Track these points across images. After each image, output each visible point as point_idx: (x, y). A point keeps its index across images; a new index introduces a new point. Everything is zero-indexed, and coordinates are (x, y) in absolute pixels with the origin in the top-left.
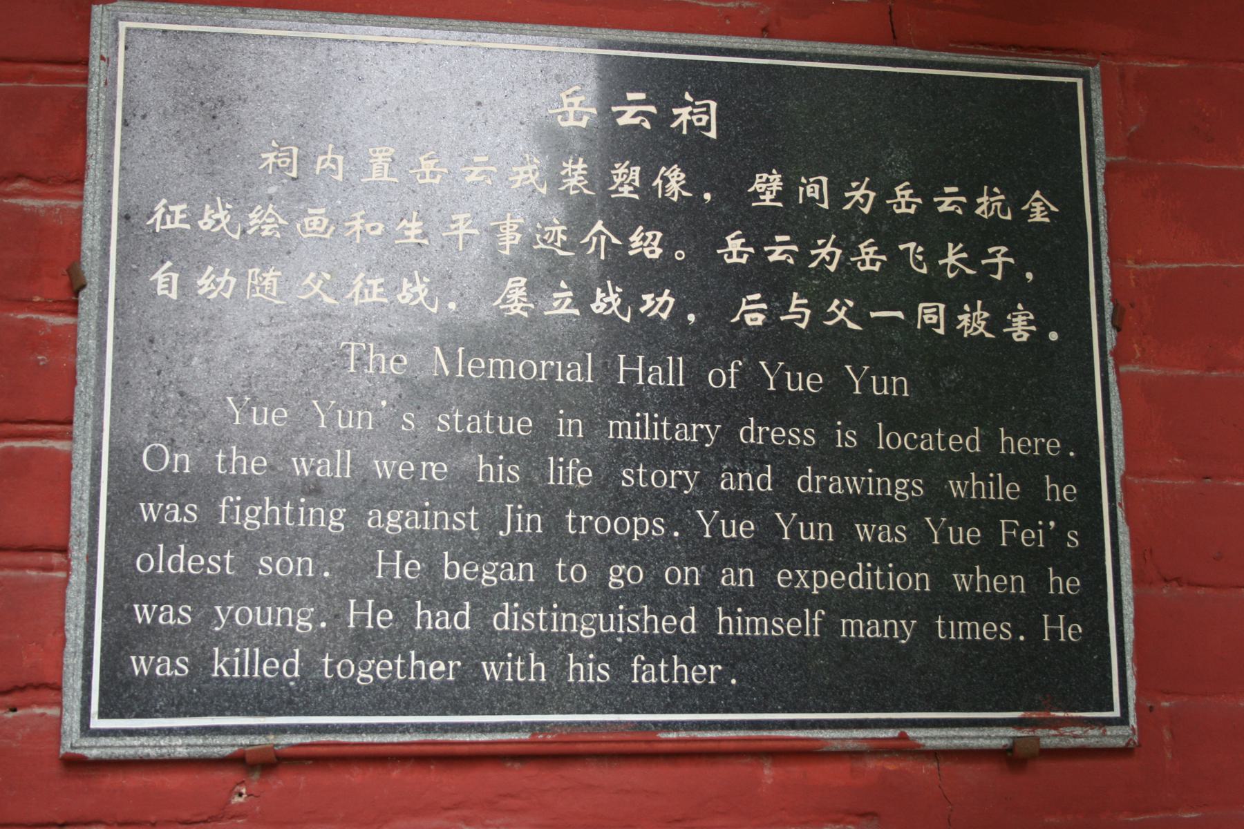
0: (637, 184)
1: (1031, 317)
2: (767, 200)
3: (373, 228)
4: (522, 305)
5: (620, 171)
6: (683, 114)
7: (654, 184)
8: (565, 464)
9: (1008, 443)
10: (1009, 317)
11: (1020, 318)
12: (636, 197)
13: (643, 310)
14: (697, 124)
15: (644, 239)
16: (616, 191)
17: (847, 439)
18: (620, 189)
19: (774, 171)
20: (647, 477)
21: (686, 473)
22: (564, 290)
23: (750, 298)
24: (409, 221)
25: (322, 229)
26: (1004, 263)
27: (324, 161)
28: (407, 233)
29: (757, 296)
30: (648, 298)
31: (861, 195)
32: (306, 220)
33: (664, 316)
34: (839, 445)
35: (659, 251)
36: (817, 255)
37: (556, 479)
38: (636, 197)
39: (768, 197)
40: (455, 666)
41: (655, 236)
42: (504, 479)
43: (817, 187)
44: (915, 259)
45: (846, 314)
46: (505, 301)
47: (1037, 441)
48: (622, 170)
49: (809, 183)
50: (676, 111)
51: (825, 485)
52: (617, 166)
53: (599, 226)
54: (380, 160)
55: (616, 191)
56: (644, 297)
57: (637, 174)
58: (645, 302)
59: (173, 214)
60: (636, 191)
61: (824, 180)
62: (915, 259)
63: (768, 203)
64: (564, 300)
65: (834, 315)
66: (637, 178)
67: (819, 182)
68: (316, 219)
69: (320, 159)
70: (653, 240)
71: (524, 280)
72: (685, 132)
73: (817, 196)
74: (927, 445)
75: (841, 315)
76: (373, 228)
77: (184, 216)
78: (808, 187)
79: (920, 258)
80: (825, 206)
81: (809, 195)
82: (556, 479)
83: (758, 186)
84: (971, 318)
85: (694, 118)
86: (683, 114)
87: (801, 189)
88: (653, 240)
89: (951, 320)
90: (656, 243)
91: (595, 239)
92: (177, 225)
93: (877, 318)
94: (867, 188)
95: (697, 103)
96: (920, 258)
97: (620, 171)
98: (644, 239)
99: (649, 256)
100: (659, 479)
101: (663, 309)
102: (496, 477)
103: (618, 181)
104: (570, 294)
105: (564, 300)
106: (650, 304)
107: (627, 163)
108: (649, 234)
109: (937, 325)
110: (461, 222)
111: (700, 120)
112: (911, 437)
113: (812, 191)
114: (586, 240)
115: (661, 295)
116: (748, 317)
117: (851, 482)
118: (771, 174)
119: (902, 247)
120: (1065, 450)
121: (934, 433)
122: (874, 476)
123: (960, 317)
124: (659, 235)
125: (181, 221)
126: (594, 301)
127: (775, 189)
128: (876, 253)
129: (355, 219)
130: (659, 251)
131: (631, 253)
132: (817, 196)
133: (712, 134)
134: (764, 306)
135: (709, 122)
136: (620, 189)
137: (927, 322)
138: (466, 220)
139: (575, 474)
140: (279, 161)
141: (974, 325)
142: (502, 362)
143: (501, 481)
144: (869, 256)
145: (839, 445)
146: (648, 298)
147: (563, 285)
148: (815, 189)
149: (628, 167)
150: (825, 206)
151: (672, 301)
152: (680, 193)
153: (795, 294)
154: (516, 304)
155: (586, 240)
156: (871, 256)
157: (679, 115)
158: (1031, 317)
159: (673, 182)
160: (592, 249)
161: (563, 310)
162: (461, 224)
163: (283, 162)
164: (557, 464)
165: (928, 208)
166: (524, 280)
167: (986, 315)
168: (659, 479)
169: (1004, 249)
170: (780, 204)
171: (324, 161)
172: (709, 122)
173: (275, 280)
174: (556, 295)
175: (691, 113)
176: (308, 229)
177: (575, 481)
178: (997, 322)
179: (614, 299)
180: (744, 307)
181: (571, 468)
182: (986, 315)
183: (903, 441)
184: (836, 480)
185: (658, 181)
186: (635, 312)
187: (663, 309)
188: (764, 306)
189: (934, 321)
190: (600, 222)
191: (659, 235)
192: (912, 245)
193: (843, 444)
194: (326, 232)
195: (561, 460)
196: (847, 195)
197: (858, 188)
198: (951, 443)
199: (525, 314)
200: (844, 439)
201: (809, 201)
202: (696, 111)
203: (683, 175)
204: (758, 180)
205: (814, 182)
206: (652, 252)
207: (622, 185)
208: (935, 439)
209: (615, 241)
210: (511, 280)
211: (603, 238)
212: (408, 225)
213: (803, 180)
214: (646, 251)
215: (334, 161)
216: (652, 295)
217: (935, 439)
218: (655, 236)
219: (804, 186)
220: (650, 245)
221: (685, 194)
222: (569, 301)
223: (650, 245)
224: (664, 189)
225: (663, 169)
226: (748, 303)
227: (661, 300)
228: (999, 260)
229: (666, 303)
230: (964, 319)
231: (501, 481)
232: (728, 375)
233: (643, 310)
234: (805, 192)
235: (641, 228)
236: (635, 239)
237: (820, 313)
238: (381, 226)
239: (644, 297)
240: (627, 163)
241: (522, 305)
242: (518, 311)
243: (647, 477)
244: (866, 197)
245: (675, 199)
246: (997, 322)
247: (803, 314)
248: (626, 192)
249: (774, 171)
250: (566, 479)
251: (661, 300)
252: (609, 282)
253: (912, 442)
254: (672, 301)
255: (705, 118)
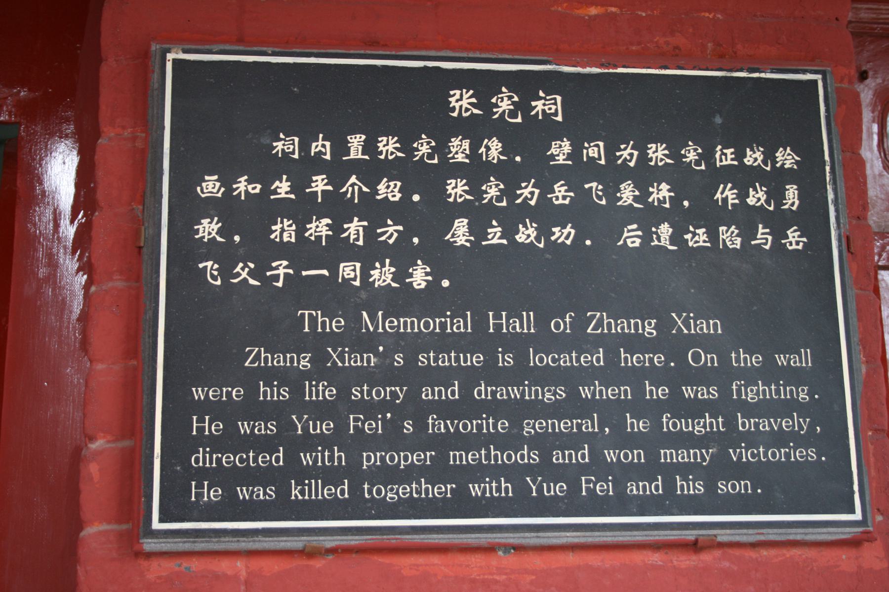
0: (468, 152)
1: (428, 270)
2: (561, 160)
3: (254, 188)
4: (465, 238)
5: (455, 144)
6: (539, 105)
7: (480, 152)
8: (317, 386)
9: (626, 359)
10: (411, 270)
11: (420, 271)
12: (467, 161)
13: (553, 238)
14: (548, 112)
15: (388, 187)
16: (453, 158)
17: (506, 360)
18: (456, 156)
19: (565, 139)
20: (369, 393)
21: (398, 388)
22: (495, 227)
23: (630, 227)
24: (281, 182)
25: (215, 191)
26: (323, 191)
27: (317, 147)
28: (279, 191)
29: (635, 226)
30: (556, 230)
31: (627, 153)
32: (204, 184)
33: (568, 242)
34: (501, 364)
35: (399, 196)
36: (522, 194)
37: (311, 396)
38: (467, 161)
39: (561, 157)
40: (431, 455)
41: (396, 185)
42: (278, 397)
43: (596, 149)
44: (597, 195)
45: (248, 274)
46: (453, 236)
47: (647, 356)
48: (457, 142)
49: (590, 147)
50: (533, 104)
51: (494, 393)
52: (453, 140)
53: (353, 179)
54: (356, 144)
55: (453, 158)
56: (554, 229)
57: (467, 144)
58: (554, 234)
59: (726, 155)
60: (467, 157)
61: (601, 144)
62: (597, 195)
63: (561, 162)
64: (496, 233)
65: (238, 274)
66: (467, 148)
67: (597, 146)
68: (211, 183)
69: (314, 145)
70: (395, 187)
71: (466, 221)
72: (540, 117)
73: (596, 156)
74: (565, 362)
75: (244, 275)
76: (254, 188)
77: (733, 156)
78: (590, 150)
79: (600, 193)
80: (603, 162)
81: (591, 155)
82: (311, 396)
83: (553, 151)
84: (381, 273)
85: (285, 147)
86: (539, 105)
87: (585, 151)
88: (395, 187)
89: (365, 274)
90: (396, 190)
91: (350, 189)
92: (729, 162)
93: (307, 276)
94: (632, 149)
95: (548, 98)
96: (600, 193)
97: (455, 144)
98: (388, 187)
99: (392, 199)
100: (378, 394)
101: (567, 238)
102: (272, 396)
103: (454, 150)
104: (500, 229)
105: (496, 233)
106: (557, 235)
107: (460, 137)
108: (392, 184)
109: (355, 279)
110: (320, 181)
111: (288, 148)
112: (553, 357)
113: (593, 152)
114: (344, 189)
115: (565, 228)
116: (629, 241)
117: (513, 390)
118: (563, 141)
119: (587, 186)
120: (667, 362)
121: (570, 353)
122: (529, 386)
123: (372, 272)
124: (399, 184)
125: (732, 160)
126: (518, 234)
127: (566, 152)
128: (566, 191)
129: (240, 182)
130: (399, 196)
131: (379, 197)
132: (596, 156)
133: (559, 118)
134: (640, 233)
135: (556, 110)
136: (456, 156)
137: (346, 277)
138: (323, 180)
139: (324, 391)
140: (285, 147)
141: (383, 277)
142: (409, 321)
143: (275, 398)
144: (561, 194)
145: (501, 364)
146: (556, 230)
147: (494, 223)
148: (595, 151)
149: (461, 140)
150: (603, 162)
151: (573, 232)
152: (498, 157)
153: (570, 225)
154: (461, 237)
155: (344, 189)
156: (563, 193)
157: (536, 106)
158: (428, 270)
159: (493, 149)
160: (349, 196)
161: (495, 241)
162: (319, 183)
163: (288, 148)
164: (311, 386)
165: (644, 158)
166: (466, 221)
167: (393, 270)
168: (378, 394)
169: (285, 263)
170: (293, 196)
171: (317, 147)
172: (556, 110)
173: (361, 229)
174: (489, 230)
175: (544, 105)
176: (205, 191)
177: (324, 396)
178: (401, 275)
179: (532, 232)
180: (626, 235)
181: (321, 388)
182: (393, 270)
183: (548, 360)
184: (502, 390)
185: (483, 150)
186: (547, 240)
187: (567, 238)
188: (640, 233)
189: (352, 275)
190: (354, 177)
191: (399, 184)
192: (594, 185)
193: (503, 363)
194: (218, 192)
195: (314, 383)
196: (518, 192)
197: (625, 149)
198: (582, 359)
199: (468, 244)
200: (504, 360)
201: (591, 159)
202: (547, 103)
203: (500, 145)
204: (553, 146)
205: (595, 146)
206: (394, 196)
207: (457, 153)
208: (571, 358)
209: (365, 189)
210: (457, 221)
211: (356, 188)
212: (280, 185)
213: (586, 145)
214: (390, 196)
215: (324, 146)
216: (559, 228)
217: (571, 358)
218: (396, 185)
219: (587, 149)
220: (392, 191)
221: (502, 157)
222: (499, 234)
223: (392, 191)
224: (487, 155)
225: (486, 141)
226: (629, 231)
227: (566, 231)
228: (281, 271)
229: (570, 233)
230: (375, 273)
231: (275, 398)
232: (565, 323)
233: (553, 238)
234: (588, 153)
235: (385, 179)
236: (381, 187)
237: (647, 237)
238: (259, 186)
239: (554, 229)
240: (460, 137)
241: (465, 238)
242: (463, 242)
243: (369, 393)
244: (631, 155)
245: (495, 161)
246: (401, 275)
247: (767, 239)
248: (460, 158)
249: (565, 139)
250: (317, 395)
251: (566, 231)
252: (527, 220)
253: (554, 360)
254: (573, 232)
255: (554, 107)
